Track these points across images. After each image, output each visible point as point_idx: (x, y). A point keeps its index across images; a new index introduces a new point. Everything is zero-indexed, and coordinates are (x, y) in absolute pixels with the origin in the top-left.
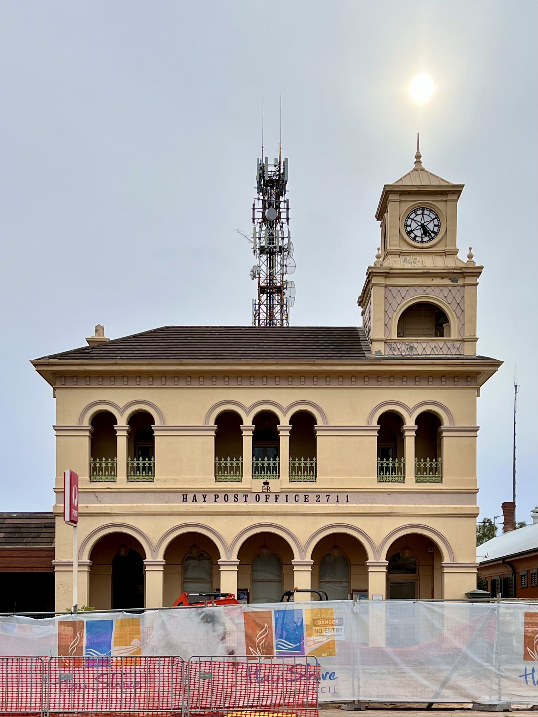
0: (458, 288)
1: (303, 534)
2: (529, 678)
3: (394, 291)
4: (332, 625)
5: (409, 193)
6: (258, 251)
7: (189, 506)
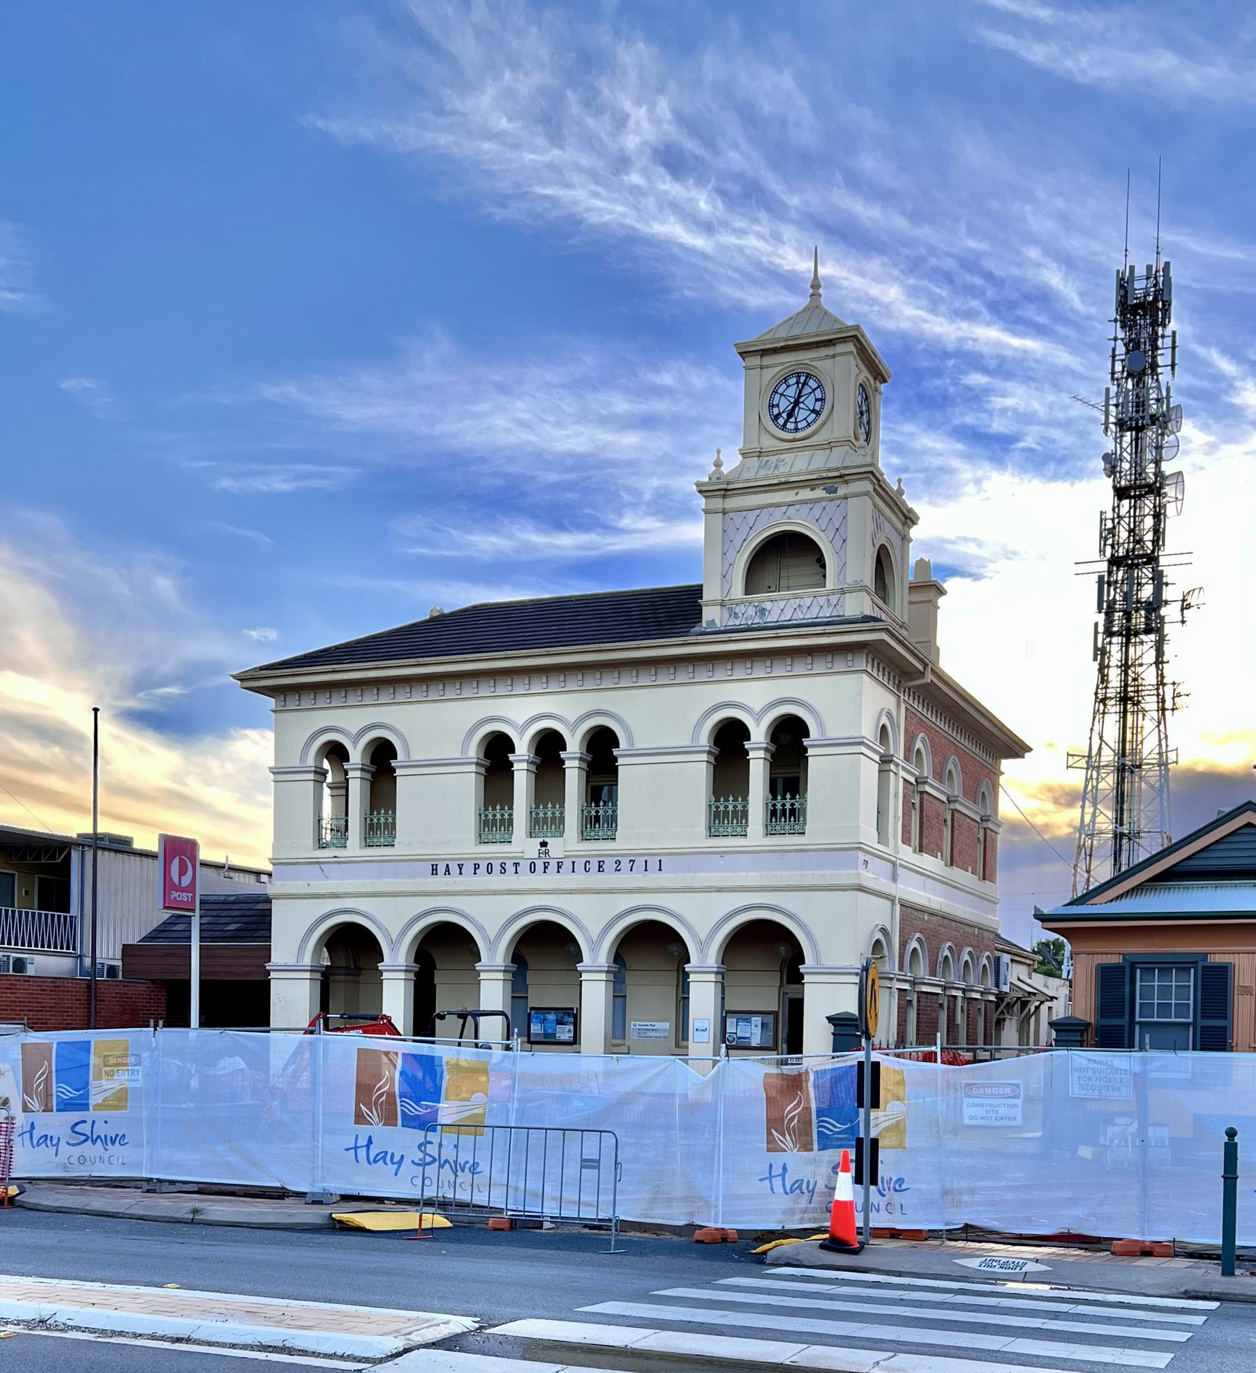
0: (838, 502)
1: (595, 924)
2: (362, 1153)
3: (738, 517)
4: (126, 1065)
5: (775, 351)
6: (1112, 427)
7: (441, 882)
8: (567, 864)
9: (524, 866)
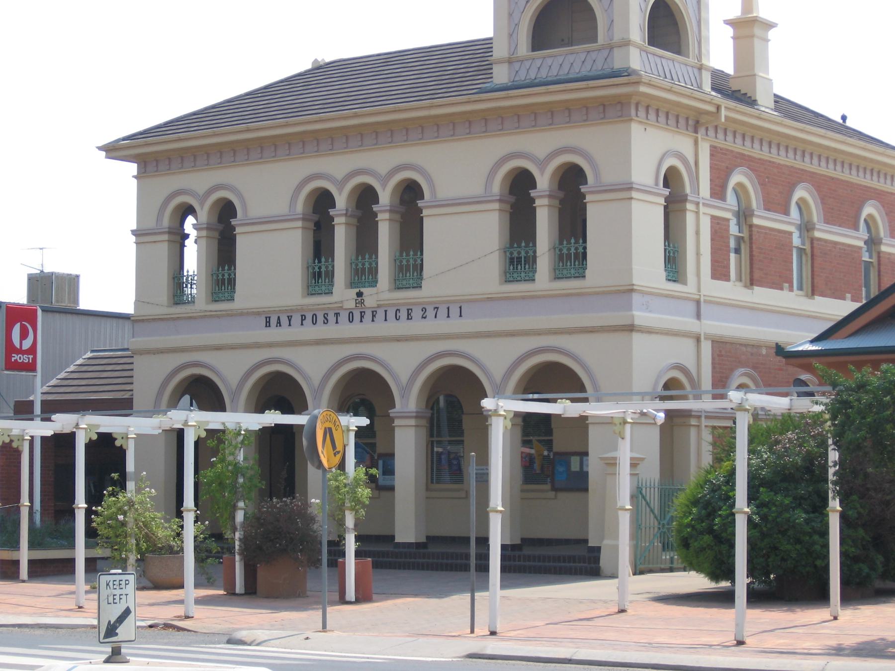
9: (344, 316)
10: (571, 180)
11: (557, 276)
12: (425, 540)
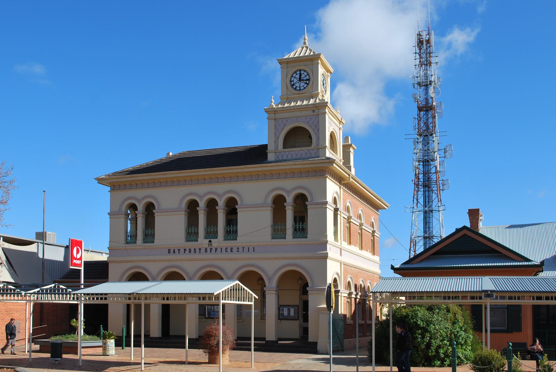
7: (171, 256)
8: (219, 250)
9: (203, 250)
10: (301, 200)
11: (145, 242)
12: (310, 340)
